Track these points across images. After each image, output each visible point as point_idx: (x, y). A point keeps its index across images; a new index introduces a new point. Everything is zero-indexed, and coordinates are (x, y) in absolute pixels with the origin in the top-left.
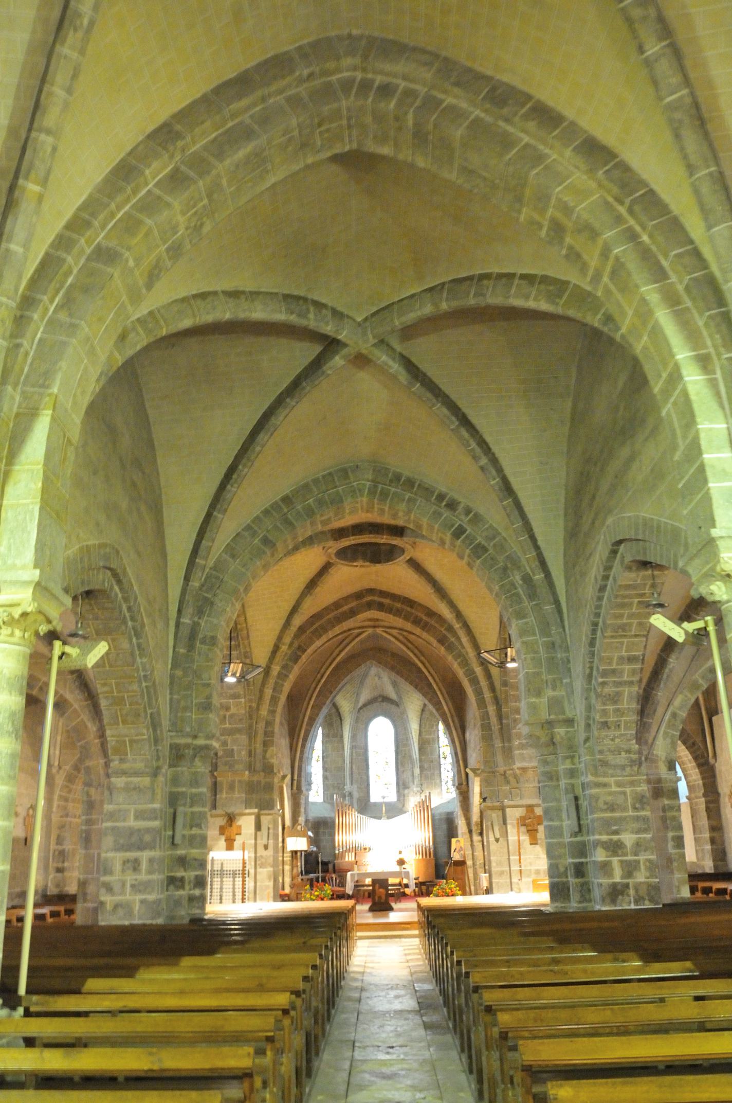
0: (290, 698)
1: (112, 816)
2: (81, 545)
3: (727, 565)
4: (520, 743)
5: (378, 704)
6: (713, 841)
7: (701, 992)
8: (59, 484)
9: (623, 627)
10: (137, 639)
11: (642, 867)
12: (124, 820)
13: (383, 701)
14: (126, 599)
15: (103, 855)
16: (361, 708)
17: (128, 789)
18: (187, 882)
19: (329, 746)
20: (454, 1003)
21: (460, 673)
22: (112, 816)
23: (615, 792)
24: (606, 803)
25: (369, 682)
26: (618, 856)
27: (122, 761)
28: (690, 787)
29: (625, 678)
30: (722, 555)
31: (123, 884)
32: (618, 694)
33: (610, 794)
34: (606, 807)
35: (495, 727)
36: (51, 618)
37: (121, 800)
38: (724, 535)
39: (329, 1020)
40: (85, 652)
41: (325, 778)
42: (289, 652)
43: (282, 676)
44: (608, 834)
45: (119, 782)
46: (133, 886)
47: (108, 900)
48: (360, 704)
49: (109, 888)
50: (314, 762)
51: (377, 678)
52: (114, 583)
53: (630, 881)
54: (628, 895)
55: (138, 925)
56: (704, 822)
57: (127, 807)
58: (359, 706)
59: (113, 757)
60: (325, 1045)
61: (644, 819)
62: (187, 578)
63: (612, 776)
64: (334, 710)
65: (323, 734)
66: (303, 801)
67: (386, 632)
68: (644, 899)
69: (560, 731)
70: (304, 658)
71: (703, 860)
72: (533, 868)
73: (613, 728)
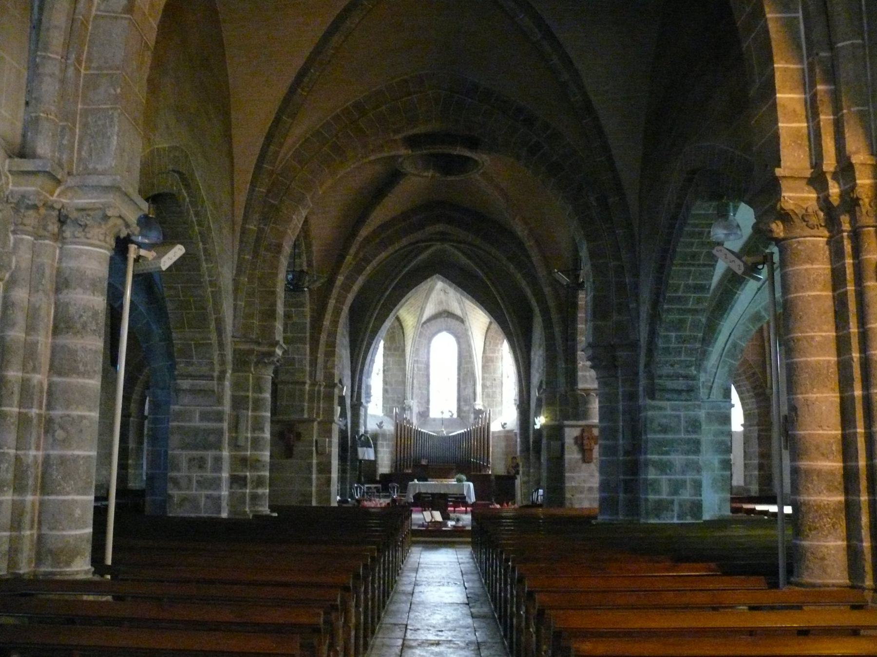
0: (352, 310)
1: (179, 416)
2: (152, 148)
3: (786, 204)
4: (583, 365)
5: (442, 319)
6: (761, 467)
7: (797, 614)
8: (137, 90)
9: (694, 256)
10: (204, 244)
11: (688, 486)
12: (190, 421)
13: (447, 317)
14: (194, 204)
15: (170, 452)
16: (425, 323)
17: (193, 391)
18: (248, 481)
19: (390, 359)
20: (500, 596)
21: (529, 292)
22: (179, 416)
23: (671, 415)
24: (659, 425)
25: (434, 297)
26: (666, 474)
27: (189, 364)
28: (747, 416)
29: (690, 306)
30: (783, 194)
31: (190, 479)
32: (682, 322)
33: (665, 416)
34: (660, 428)
35: (560, 349)
36: (129, 222)
37: (186, 401)
38: (787, 175)
39: (384, 607)
40: (160, 257)
41: (385, 391)
42: (354, 263)
43: (346, 288)
44: (659, 454)
45: (185, 384)
46: (198, 482)
47: (175, 493)
48: (424, 319)
49: (176, 482)
50: (374, 375)
51: (442, 293)
52: (182, 187)
53: (675, 497)
54: (673, 511)
55: (204, 518)
56: (755, 449)
57: (192, 408)
58: (423, 321)
59: (179, 360)
60: (379, 629)
61: (694, 442)
62: (253, 184)
63: (668, 400)
64: (397, 324)
65: (385, 348)
66: (362, 413)
67: (456, 247)
68: (686, 514)
69: (622, 354)
70: (369, 269)
71: (750, 483)
72: (587, 485)
73: (673, 354)
